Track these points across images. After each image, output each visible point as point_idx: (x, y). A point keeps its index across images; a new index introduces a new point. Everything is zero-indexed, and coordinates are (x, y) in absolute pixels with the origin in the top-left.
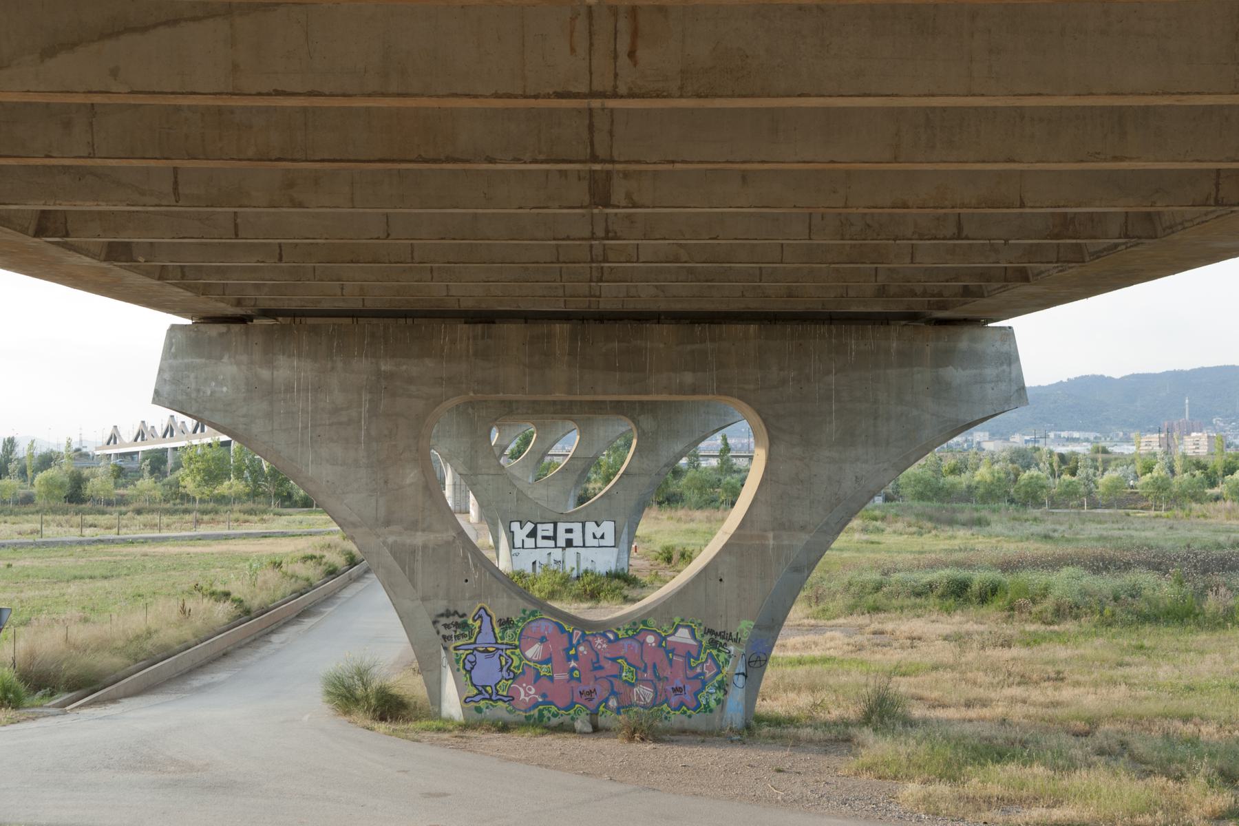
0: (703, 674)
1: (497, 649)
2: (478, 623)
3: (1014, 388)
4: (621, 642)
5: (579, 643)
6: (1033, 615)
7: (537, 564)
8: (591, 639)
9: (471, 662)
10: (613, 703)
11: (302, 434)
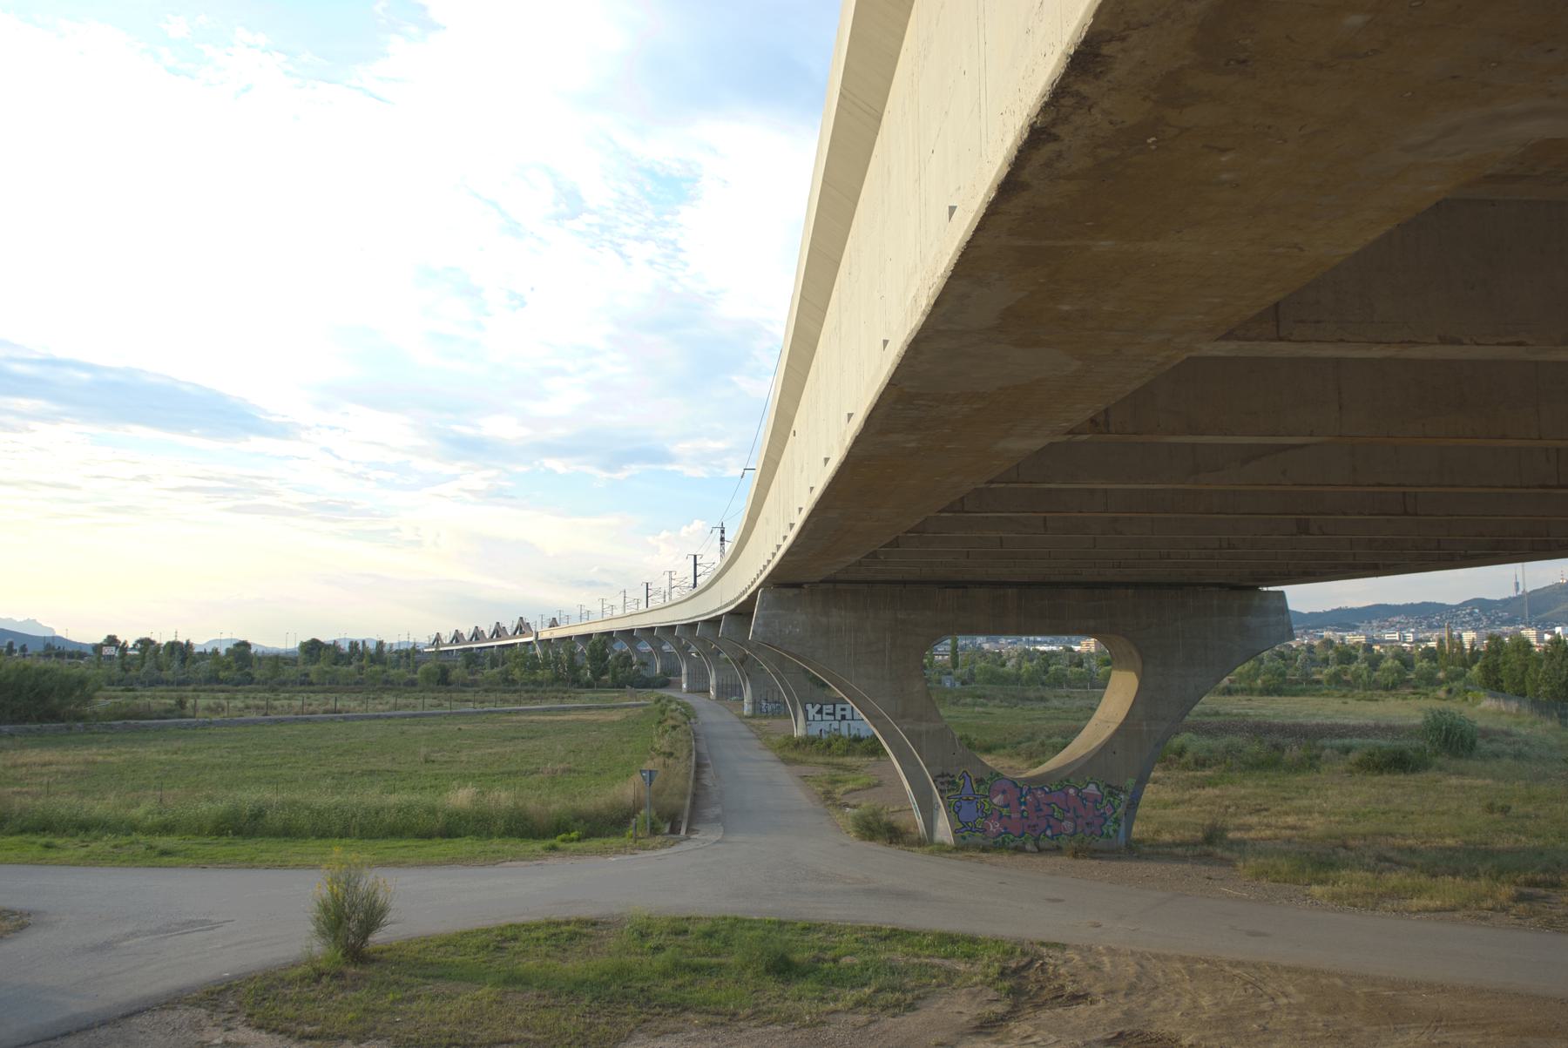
0: (1105, 813)
5: (1026, 794)
8: (1034, 791)
10: (1049, 832)
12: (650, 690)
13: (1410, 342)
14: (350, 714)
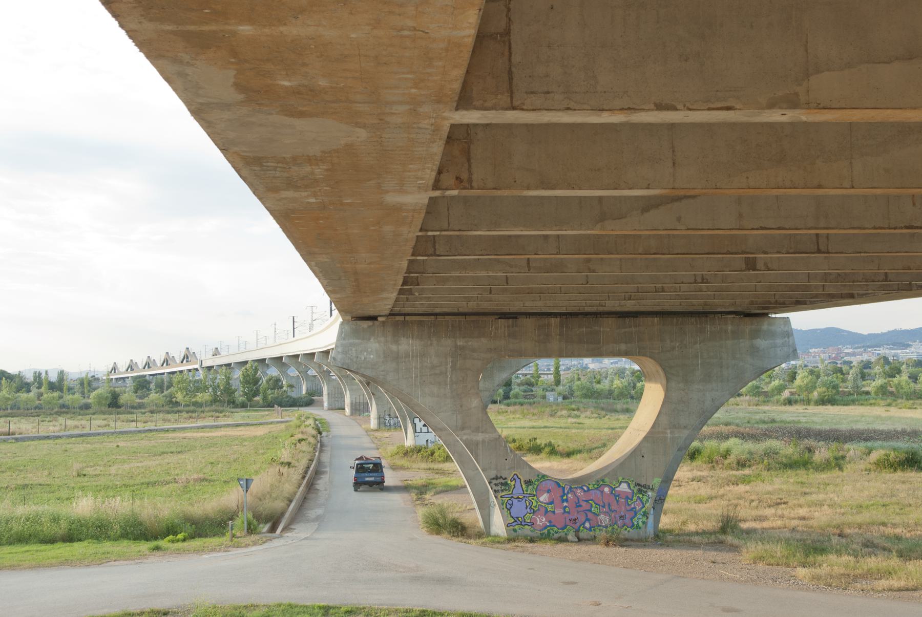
0: (635, 508)
1: (524, 497)
2: (513, 482)
3: (791, 350)
4: (591, 492)
5: (568, 493)
6: (725, 466)
7: (429, 442)
8: (574, 490)
9: (510, 504)
11: (415, 380)
12: (296, 408)
13: (629, 109)
14: (23, 435)
